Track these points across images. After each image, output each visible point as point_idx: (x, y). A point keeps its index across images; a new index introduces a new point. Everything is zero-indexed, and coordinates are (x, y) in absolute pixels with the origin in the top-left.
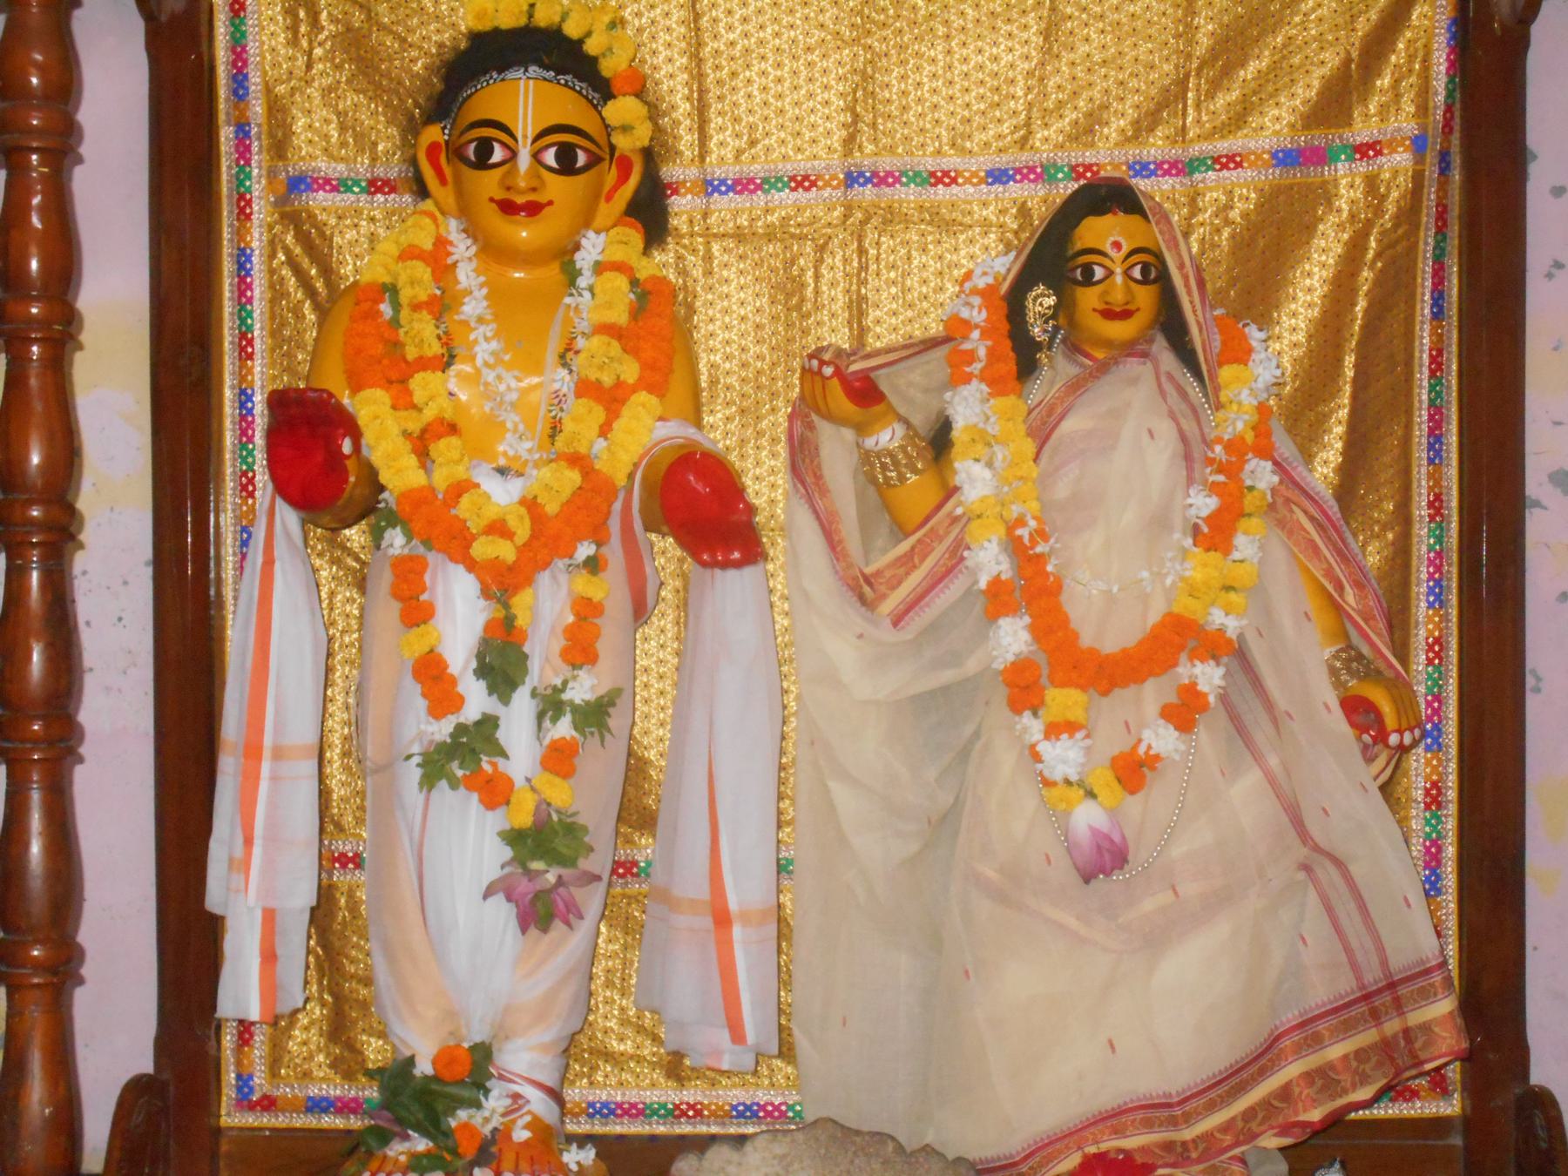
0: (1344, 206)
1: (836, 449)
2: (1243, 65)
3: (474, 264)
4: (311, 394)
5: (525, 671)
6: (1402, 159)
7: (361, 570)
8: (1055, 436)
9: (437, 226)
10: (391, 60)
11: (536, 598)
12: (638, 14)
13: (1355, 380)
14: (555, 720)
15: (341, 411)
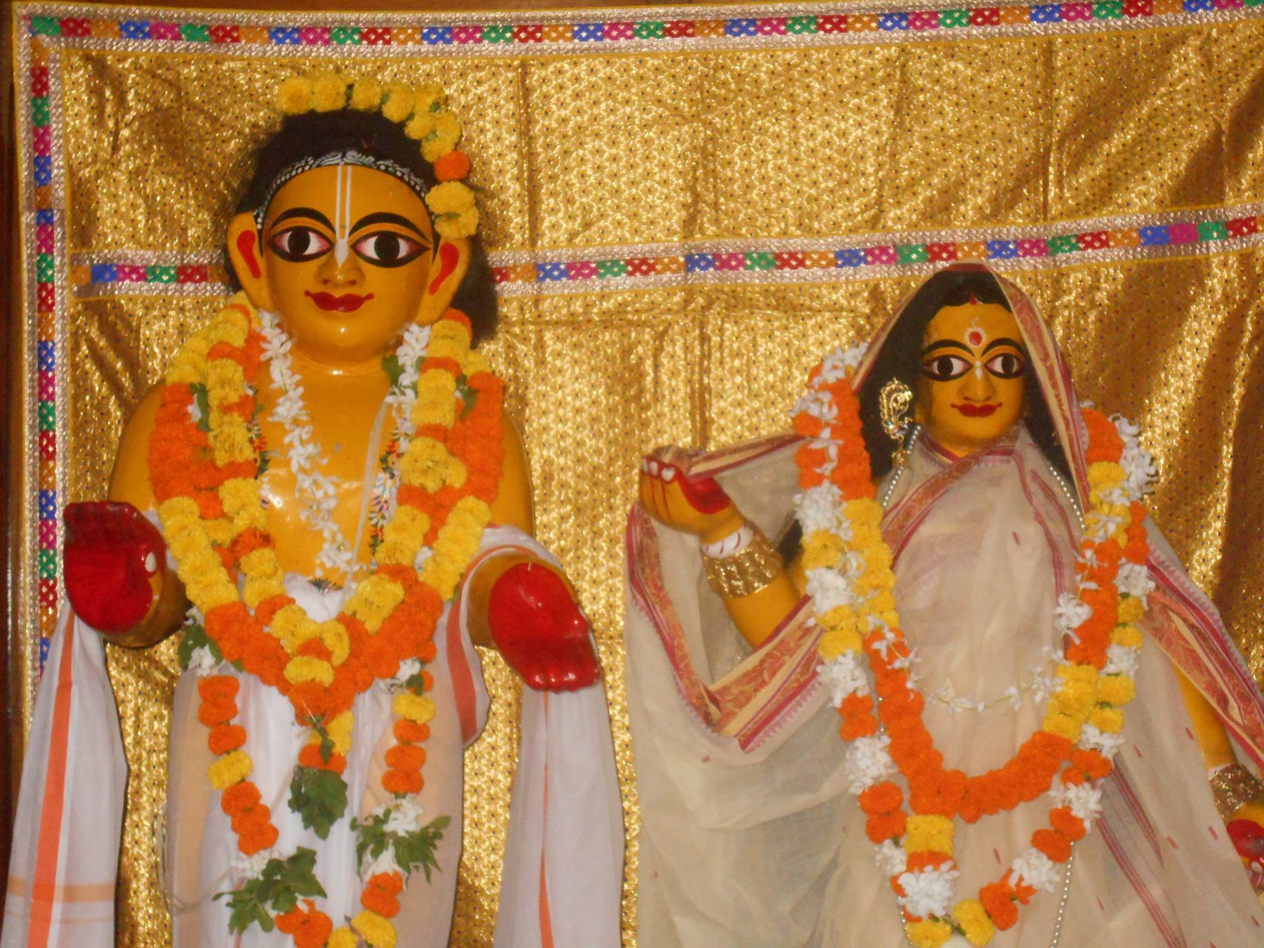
0: (1217, 287)
1: (678, 554)
2: (1107, 139)
4: (110, 508)
5: (344, 802)
9: (250, 321)
10: (201, 140)
11: (356, 720)
13: (1233, 472)
14: (376, 854)
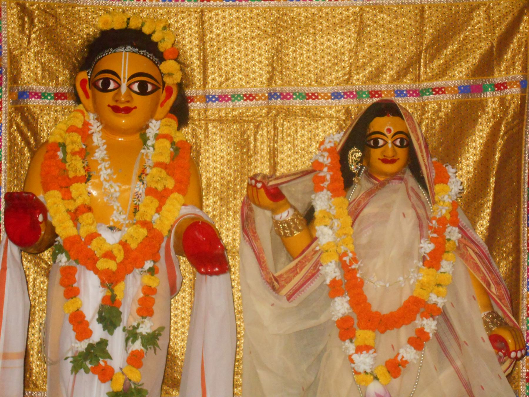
0: (490, 111)
1: (263, 219)
2: (446, 47)
3: (101, 134)
4: (24, 195)
5: (120, 320)
6: (516, 90)
7: (48, 269)
8: (361, 215)
9: (84, 117)
10: (66, 40)
12: (177, 22)
14: (133, 342)
15: (38, 201)
